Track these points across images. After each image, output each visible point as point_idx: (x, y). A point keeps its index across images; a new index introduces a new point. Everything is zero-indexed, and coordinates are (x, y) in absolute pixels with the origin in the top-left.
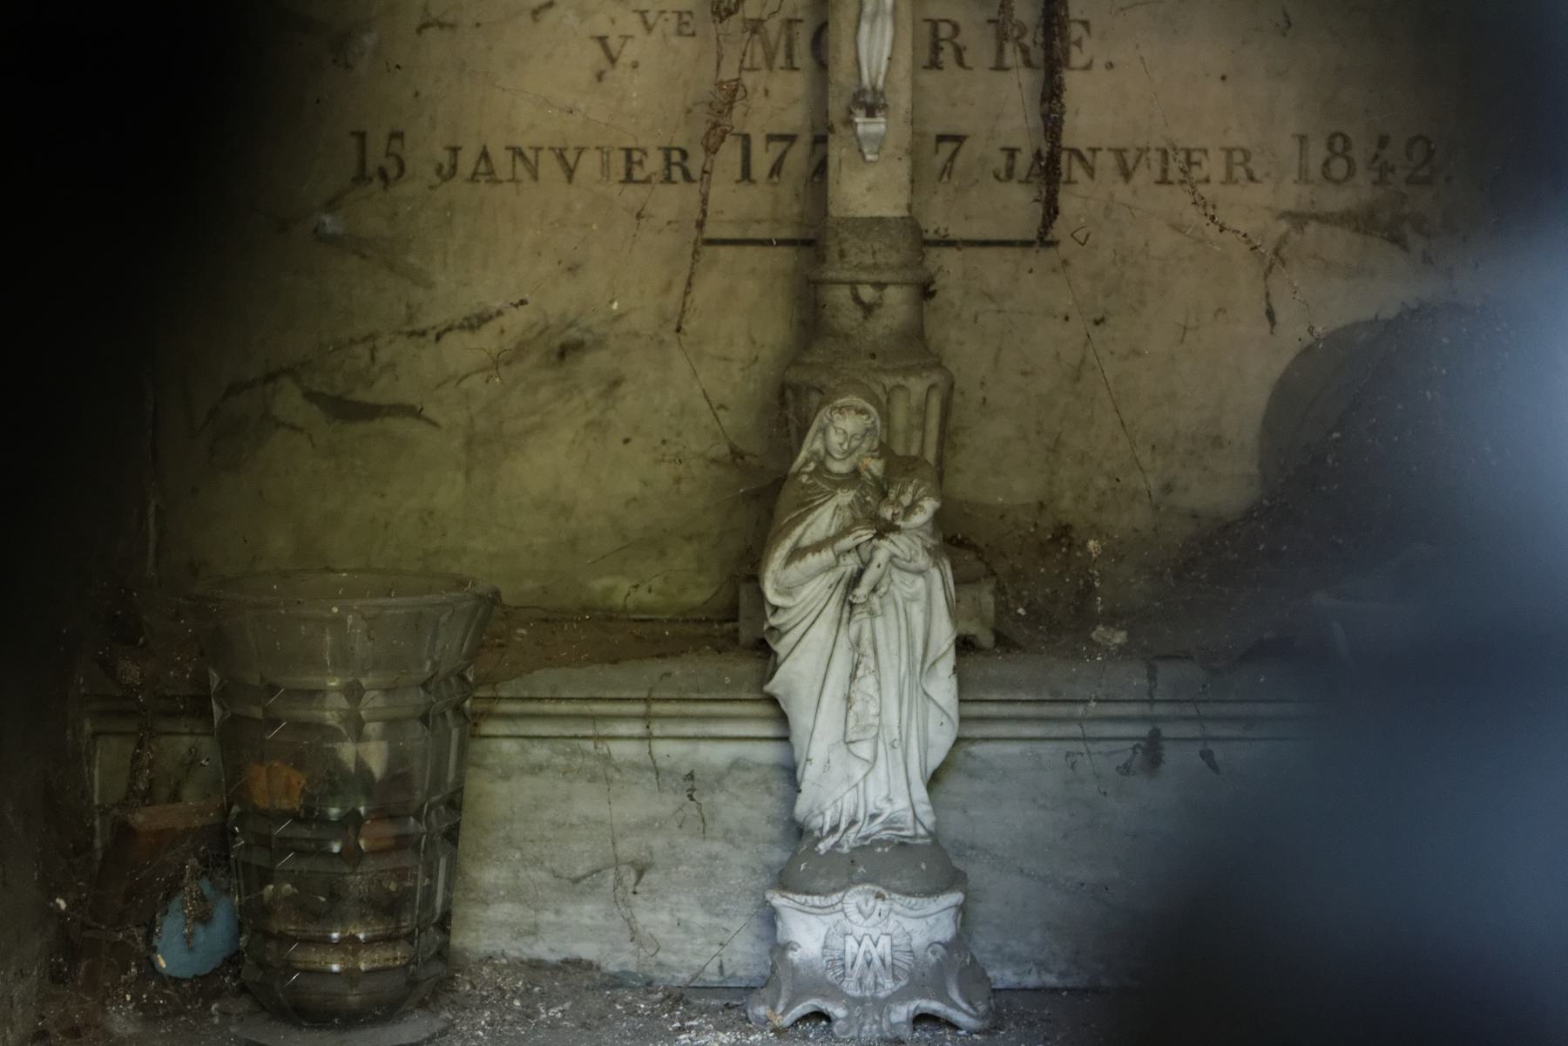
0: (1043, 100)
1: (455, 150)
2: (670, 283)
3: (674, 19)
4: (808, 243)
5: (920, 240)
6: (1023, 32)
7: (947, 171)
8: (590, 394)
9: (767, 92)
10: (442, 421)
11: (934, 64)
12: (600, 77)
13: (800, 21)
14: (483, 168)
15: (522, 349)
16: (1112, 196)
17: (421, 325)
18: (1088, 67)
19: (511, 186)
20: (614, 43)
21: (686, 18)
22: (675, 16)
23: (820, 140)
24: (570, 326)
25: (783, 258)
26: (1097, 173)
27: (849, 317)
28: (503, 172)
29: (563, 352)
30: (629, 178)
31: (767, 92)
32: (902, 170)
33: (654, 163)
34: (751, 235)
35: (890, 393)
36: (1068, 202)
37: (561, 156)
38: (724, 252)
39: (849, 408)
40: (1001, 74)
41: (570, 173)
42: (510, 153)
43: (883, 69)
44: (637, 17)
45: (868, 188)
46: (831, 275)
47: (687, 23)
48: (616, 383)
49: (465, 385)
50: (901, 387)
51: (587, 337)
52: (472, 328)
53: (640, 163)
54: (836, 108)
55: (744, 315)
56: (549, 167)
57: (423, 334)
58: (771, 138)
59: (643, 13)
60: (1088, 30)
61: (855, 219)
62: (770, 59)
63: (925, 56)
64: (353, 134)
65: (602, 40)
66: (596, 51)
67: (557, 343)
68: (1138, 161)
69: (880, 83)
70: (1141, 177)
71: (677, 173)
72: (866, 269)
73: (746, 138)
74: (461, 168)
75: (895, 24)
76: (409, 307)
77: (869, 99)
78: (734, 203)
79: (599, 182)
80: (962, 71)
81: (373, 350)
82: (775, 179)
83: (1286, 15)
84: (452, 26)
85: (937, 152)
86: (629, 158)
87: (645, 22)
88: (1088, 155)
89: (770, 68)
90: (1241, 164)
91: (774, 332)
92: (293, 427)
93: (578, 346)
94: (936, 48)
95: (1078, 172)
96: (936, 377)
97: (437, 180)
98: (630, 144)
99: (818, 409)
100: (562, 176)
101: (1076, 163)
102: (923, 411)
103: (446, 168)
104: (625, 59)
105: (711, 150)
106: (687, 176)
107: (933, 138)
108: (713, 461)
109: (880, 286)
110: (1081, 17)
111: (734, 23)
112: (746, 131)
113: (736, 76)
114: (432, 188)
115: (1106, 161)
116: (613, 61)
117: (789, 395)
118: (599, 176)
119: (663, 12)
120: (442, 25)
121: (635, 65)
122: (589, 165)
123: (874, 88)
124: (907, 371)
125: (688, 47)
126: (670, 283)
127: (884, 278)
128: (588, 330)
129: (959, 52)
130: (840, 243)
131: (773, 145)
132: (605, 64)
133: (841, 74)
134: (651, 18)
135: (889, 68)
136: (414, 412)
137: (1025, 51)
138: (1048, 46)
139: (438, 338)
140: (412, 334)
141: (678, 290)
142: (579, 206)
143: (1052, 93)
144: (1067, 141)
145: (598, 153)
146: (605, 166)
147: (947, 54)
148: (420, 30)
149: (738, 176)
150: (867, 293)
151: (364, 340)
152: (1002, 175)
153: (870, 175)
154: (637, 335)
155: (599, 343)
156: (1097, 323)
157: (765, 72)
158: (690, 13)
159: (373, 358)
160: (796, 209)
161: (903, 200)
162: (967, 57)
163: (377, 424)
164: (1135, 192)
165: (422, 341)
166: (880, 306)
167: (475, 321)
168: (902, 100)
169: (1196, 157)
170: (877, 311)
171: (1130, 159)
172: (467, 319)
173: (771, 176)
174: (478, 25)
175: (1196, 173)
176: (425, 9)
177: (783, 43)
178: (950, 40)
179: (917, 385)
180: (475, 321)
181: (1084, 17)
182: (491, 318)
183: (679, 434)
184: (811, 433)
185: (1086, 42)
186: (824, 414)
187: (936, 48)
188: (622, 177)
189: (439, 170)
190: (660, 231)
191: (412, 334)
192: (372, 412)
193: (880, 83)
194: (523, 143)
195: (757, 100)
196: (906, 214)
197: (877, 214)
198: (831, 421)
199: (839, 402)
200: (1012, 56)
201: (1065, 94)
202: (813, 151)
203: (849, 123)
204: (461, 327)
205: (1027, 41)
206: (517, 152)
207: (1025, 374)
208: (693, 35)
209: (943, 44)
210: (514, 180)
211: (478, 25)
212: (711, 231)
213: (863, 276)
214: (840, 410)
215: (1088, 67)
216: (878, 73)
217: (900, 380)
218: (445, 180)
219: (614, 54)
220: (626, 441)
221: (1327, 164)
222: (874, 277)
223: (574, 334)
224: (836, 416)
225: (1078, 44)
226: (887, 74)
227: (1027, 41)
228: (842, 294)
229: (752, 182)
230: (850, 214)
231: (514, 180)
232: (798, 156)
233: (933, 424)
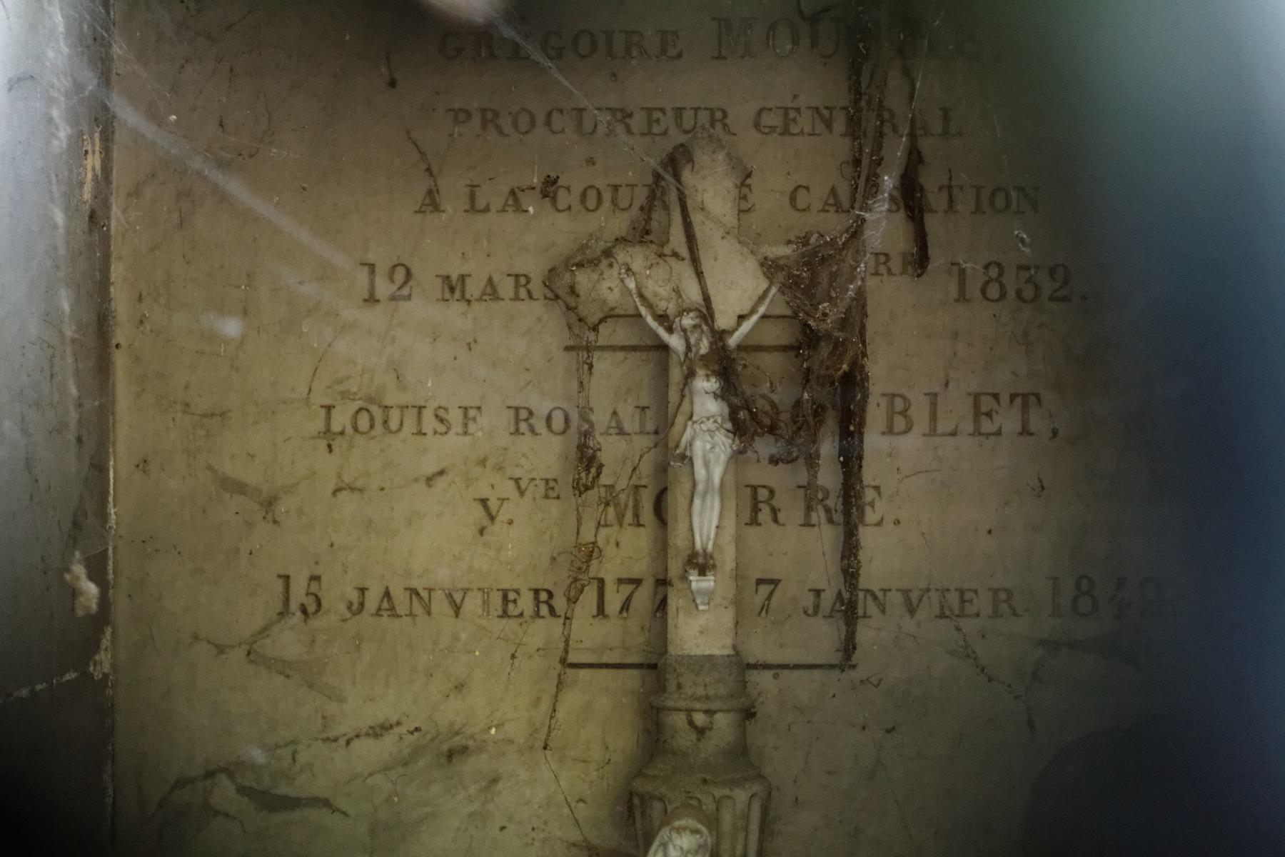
0: (843, 557)
1: (362, 590)
2: (539, 699)
3: (542, 485)
4: (653, 667)
5: (742, 666)
6: (827, 494)
7: (765, 608)
8: (473, 789)
9: (618, 544)
10: (351, 811)
11: (754, 522)
12: (482, 531)
13: (645, 486)
14: (385, 605)
15: (416, 752)
16: (900, 627)
17: (332, 734)
18: (879, 524)
19: (409, 619)
20: (493, 504)
21: (552, 484)
22: (543, 483)
23: (663, 582)
24: (457, 734)
25: (631, 679)
26: (888, 611)
27: (685, 739)
28: (402, 609)
29: (450, 755)
30: (505, 614)
31: (618, 544)
32: (728, 617)
33: (526, 603)
34: (605, 660)
35: (718, 803)
36: (865, 634)
37: (450, 596)
38: (583, 673)
39: (684, 829)
40: (807, 529)
41: (457, 609)
42: (408, 593)
43: (712, 536)
44: (512, 483)
45: (702, 629)
46: (670, 703)
47: (553, 488)
48: (495, 781)
49: (370, 781)
50: (729, 797)
51: (471, 743)
52: (376, 736)
53: (515, 601)
54: (675, 568)
55: (599, 719)
56: (440, 605)
57: (335, 740)
58: (621, 581)
59: (517, 481)
60: (879, 494)
61: (690, 657)
62: (620, 519)
63: (746, 517)
64: (280, 576)
65: (484, 502)
66: (479, 512)
67: (445, 747)
68: (920, 600)
69: (710, 547)
70: (921, 614)
71: (544, 610)
72: (699, 699)
73: (601, 582)
74: (367, 605)
75: (722, 500)
76: (324, 717)
77: (701, 560)
78: (590, 634)
79: (480, 617)
80: (775, 526)
81: (294, 754)
82: (625, 614)
83: (1040, 480)
84: (361, 490)
85: (758, 593)
86: (505, 597)
87: (519, 488)
88: (880, 594)
89: (621, 525)
90: (1005, 601)
91: (625, 741)
92: (227, 815)
93: (464, 750)
94: (755, 510)
95: (872, 609)
96: (757, 788)
97: (349, 615)
98: (505, 586)
99: (659, 830)
100: (451, 613)
101: (870, 601)
102: (746, 817)
103: (356, 606)
104: (503, 517)
105: (572, 600)
106: (552, 611)
107: (753, 582)
108: (574, 845)
109: (710, 713)
110: (873, 483)
111: (593, 495)
112: (601, 575)
113: (593, 540)
114: (344, 620)
115: (895, 598)
116: (492, 519)
117: (636, 801)
118: (480, 611)
119: (534, 479)
120: (352, 489)
121: (510, 522)
122: (472, 604)
123: (705, 551)
124: (732, 783)
125: (554, 507)
126: (539, 699)
127: (714, 706)
128: (472, 737)
129: (774, 511)
130: (677, 677)
131: (623, 587)
132: (486, 522)
133: (678, 538)
134: (523, 484)
135: (717, 534)
136: (326, 803)
137: (828, 510)
138: (847, 514)
139: (348, 743)
140: (326, 740)
141: (545, 706)
142: (464, 636)
143: (850, 549)
144: (863, 583)
145: (480, 594)
146: (486, 603)
147: (765, 515)
148: (335, 493)
149: (595, 612)
150: (699, 719)
151: (287, 745)
152: (810, 612)
153: (702, 620)
154: (511, 742)
155: (480, 749)
156: (889, 731)
157: (616, 528)
158: (555, 480)
159: (294, 760)
160: (641, 639)
161: (729, 642)
162: (781, 516)
163: (295, 815)
164: (919, 624)
165: (334, 745)
166: (711, 729)
167: (378, 730)
168: (727, 559)
169: (968, 596)
170: (708, 733)
171: (915, 596)
172: (371, 727)
173: (621, 612)
174: (382, 489)
175: (970, 609)
176: (339, 476)
177: (631, 504)
178: (767, 502)
179: (741, 795)
180: (378, 730)
181: (876, 483)
182: (391, 727)
183: (545, 823)
184: (654, 847)
185: (878, 504)
186: (664, 833)
187: (755, 510)
188: (500, 613)
189: (350, 607)
190: (530, 657)
191: (326, 740)
192: (293, 803)
193: (710, 547)
194: (415, 583)
195: (610, 551)
196: (731, 652)
197: (708, 652)
198: (670, 839)
199: (677, 824)
200: (819, 515)
201: (861, 553)
202: (656, 593)
203: (684, 578)
204: (367, 734)
205: (830, 503)
206: (414, 592)
207: (829, 773)
208: (558, 497)
209: (761, 506)
210: (411, 615)
211: (382, 489)
212: (572, 658)
213: (698, 705)
214: (679, 830)
215: (879, 524)
216: (708, 539)
217: (727, 792)
218: (354, 615)
219: (494, 513)
220: (503, 828)
221: (1075, 600)
222: (705, 706)
223: (458, 741)
224: (675, 835)
225: (872, 504)
226: (716, 539)
227: (830, 503)
228: (679, 719)
229: (606, 616)
230: (686, 652)
231: (411, 615)
232: (644, 596)
233: (754, 827)
